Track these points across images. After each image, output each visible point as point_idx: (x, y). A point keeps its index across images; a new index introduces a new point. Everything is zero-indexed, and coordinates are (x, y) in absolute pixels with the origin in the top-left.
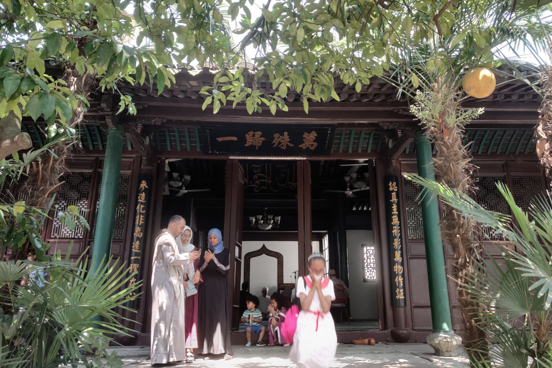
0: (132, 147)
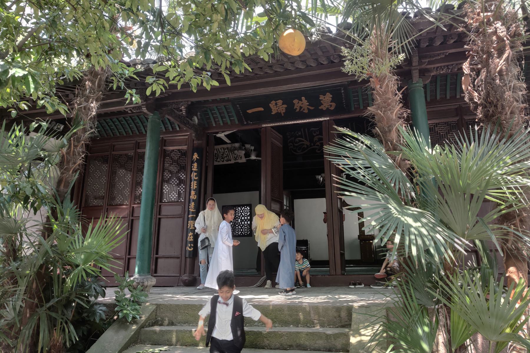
0: (180, 128)
